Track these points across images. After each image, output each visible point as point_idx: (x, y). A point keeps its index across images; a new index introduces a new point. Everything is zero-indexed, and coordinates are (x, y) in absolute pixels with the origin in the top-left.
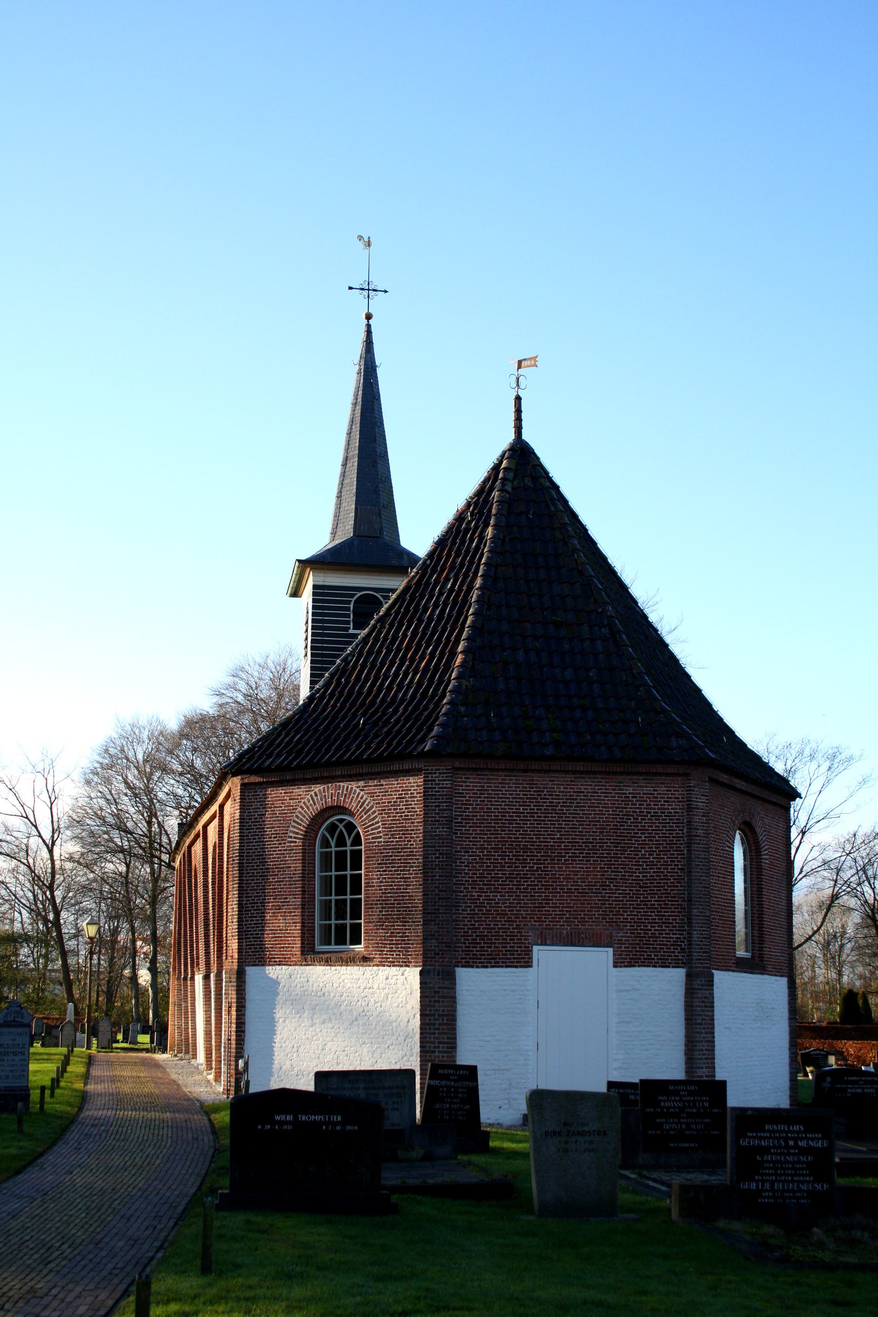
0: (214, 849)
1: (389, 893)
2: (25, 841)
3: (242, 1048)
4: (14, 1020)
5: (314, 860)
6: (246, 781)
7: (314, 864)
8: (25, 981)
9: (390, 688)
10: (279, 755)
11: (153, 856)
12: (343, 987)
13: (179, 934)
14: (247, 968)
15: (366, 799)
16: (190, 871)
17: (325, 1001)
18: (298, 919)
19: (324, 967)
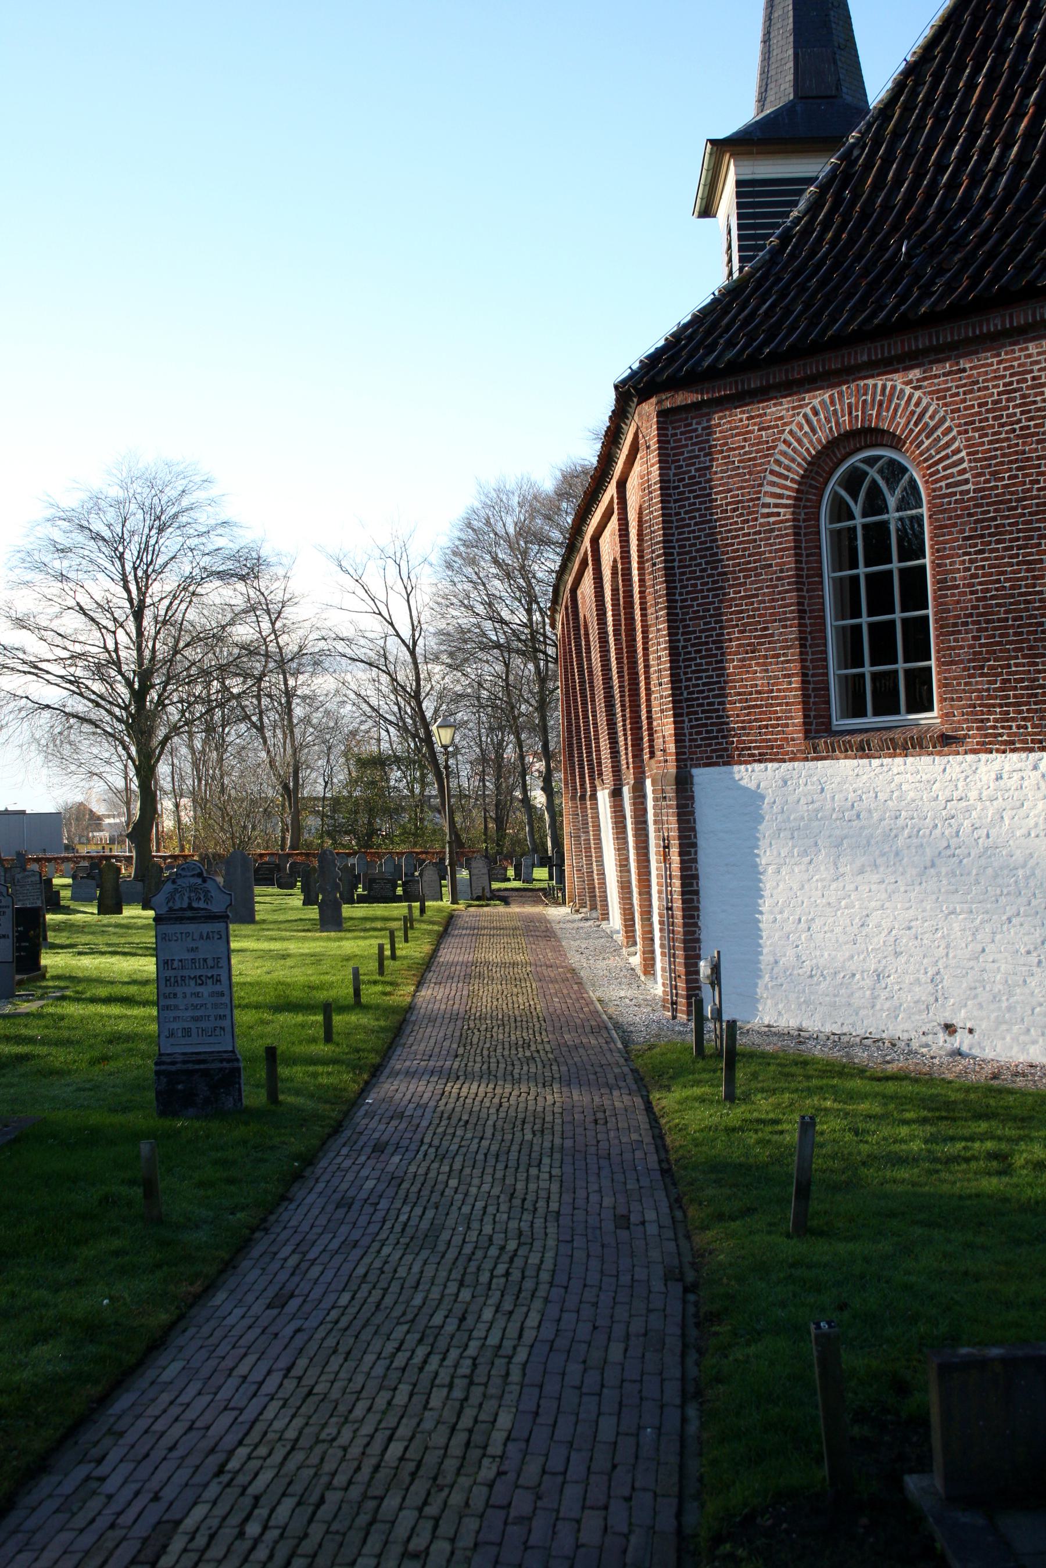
0: (614, 573)
1: (992, 598)
2: (381, 642)
3: (696, 925)
4: (190, 907)
5: (819, 547)
6: (668, 405)
7: (820, 555)
8: (399, 810)
9: (953, 184)
10: (731, 344)
11: (537, 650)
12: (901, 799)
13: (570, 731)
14: (695, 771)
15: (928, 405)
16: (577, 628)
17: (862, 828)
18: (795, 668)
19: (855, 762)
